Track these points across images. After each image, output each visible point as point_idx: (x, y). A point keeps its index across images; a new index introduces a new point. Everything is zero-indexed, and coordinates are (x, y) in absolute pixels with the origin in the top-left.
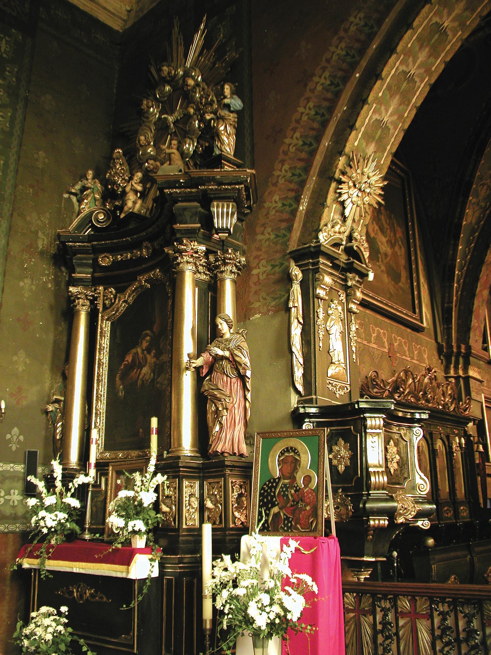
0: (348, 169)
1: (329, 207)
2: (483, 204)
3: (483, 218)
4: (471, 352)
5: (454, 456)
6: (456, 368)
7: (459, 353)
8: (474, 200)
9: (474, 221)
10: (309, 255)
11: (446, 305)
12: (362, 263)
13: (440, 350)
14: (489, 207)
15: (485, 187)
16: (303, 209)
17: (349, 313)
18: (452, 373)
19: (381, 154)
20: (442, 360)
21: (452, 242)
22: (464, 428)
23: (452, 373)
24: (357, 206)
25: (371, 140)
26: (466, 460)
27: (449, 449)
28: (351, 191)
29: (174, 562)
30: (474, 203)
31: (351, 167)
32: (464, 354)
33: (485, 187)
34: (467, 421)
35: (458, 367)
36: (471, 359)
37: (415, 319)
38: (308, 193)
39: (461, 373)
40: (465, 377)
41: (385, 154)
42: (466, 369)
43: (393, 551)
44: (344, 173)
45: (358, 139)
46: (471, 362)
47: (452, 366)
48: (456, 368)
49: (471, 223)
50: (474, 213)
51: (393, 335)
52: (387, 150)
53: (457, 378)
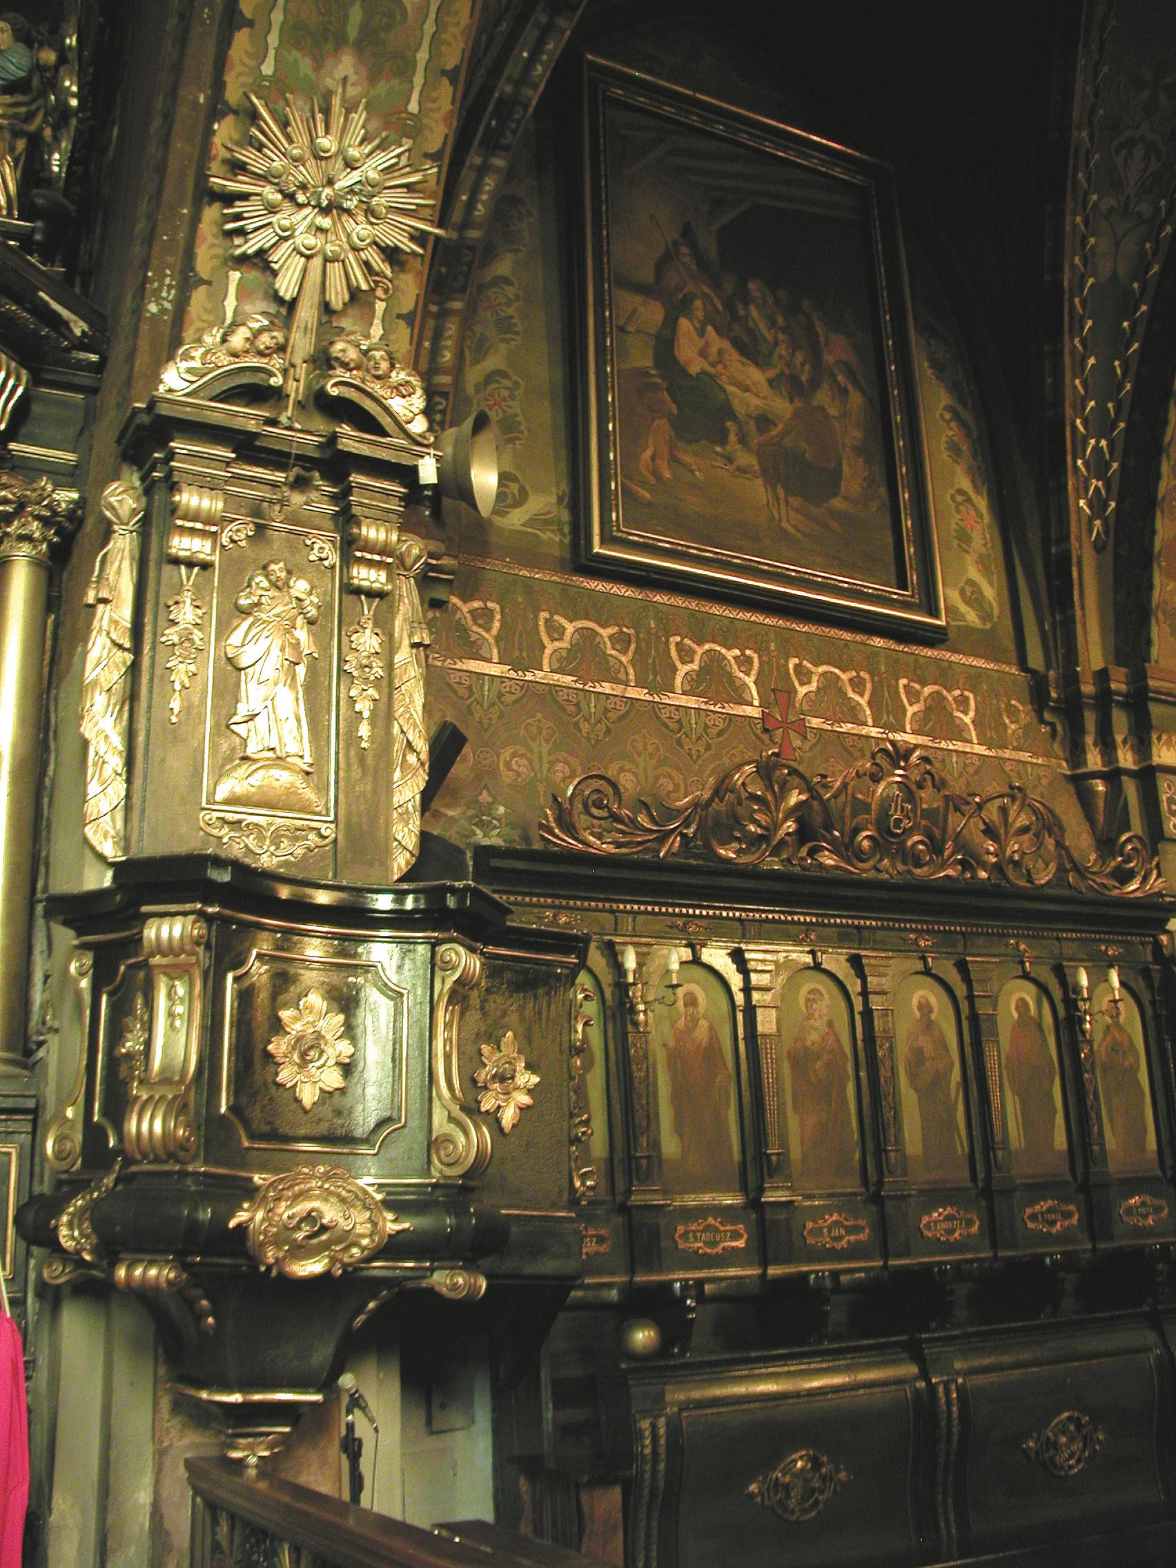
0: (247, 156)
1: (209, 283)
2: (1145, 209)
3: (1155, 253)
4: (1146, 688)
5: (1083, 1032)
6: (1107, 746)
7: (1104, 699)
8: (1109, 202)
9: (1123, 270)
10: (148, 441)
11: (1053, 549)
12: (385, 434)
13: (1038, 695)
14: (1169, 213)
15: (1139, 152)
16: (163, 311)
17: (349, 599)
18: (1094, 760)
19: (395, 82)
20: (1052, 725)
21: (1047, 348)
22: (1154, 936)
23: (1094, 760)
24: (326, 260)
25: (329, 46)
26: (1160, 1043)
27: (1067, 1009)
28: (282, 219)
29: (792, 1401)
30: (1111, 211)
31: (260, 147)
32: (1127, 695)
33: (1139, 152)
34: (1161, 915)
35: (1114, 741)
36: (1155, 709)
37: (904, 605)
38: (170, 259)
39: (1126, 759)
40: (1140, 770)
41: (418, 80)
42: (1142, 747)
43: (632, 1356)
44: (238, 167)
45: (272, 53)
46: (1154, 722)
47: (1089, 740)
48: (1107, 746)
49: (1114, 277)
50: (1117, 244)
51: (903, 682)
52: (421, 66)
53: (1113, 776)
